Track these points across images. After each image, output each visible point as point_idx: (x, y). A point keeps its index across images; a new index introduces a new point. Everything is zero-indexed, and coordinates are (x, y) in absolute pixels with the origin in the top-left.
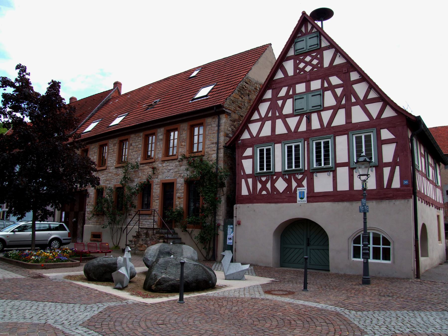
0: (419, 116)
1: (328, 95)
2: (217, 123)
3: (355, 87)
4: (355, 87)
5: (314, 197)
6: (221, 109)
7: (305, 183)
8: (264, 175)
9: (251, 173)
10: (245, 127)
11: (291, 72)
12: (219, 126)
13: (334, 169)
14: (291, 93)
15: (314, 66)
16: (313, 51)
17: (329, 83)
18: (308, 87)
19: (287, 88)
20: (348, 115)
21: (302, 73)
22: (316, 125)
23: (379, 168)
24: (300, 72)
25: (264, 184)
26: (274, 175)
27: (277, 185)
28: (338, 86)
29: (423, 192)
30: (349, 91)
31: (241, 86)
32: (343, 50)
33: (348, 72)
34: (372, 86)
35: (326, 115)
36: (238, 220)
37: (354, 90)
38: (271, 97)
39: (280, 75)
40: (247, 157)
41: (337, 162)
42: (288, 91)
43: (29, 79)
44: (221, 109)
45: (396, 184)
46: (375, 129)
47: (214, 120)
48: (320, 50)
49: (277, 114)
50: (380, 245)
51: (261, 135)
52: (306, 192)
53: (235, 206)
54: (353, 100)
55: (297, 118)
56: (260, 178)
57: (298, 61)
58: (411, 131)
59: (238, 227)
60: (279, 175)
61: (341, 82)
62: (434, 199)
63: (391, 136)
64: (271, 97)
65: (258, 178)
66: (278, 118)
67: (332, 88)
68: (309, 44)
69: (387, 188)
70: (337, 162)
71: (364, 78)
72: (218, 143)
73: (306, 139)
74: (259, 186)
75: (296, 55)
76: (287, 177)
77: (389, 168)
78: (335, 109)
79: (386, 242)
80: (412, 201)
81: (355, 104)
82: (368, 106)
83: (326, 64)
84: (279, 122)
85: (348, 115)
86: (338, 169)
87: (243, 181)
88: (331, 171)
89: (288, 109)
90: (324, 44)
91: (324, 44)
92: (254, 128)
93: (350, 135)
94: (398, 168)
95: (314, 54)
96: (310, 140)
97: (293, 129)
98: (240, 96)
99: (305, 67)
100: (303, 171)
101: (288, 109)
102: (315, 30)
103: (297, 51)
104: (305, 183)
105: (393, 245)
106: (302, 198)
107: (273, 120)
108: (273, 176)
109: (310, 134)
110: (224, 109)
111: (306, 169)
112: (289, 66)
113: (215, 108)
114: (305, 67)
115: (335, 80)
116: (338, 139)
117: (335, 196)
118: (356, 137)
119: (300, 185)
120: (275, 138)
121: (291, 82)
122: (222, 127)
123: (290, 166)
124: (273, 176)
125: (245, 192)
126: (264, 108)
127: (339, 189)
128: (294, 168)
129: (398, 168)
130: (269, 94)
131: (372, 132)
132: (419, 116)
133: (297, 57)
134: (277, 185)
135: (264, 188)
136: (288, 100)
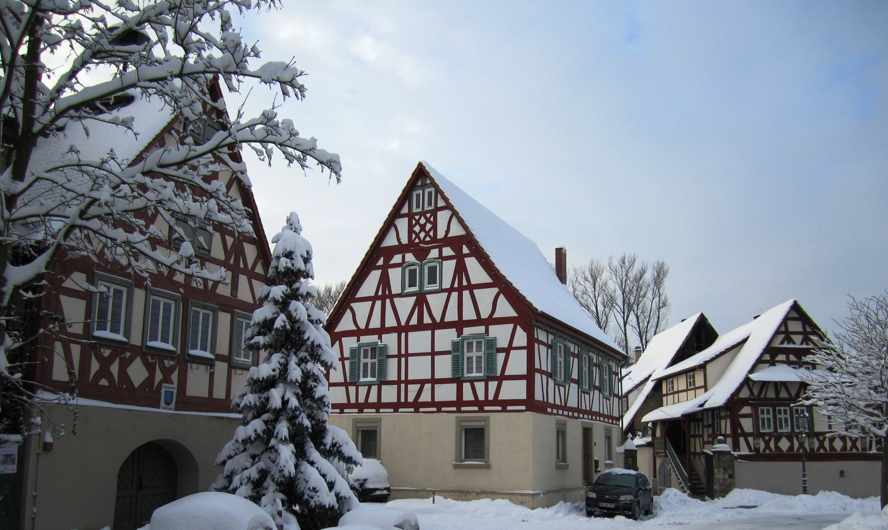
5: (185, 402)
7: (175, 376)
25: (105, 363)
41: (81, 333)
43: (324, 422)
52: (175, 391)
74: (95, 366)
87: (58, 346)
104: (175, 376)
106: (168, 403)
119: (167, 379)
127: (430, 332)
129: (499, 374)
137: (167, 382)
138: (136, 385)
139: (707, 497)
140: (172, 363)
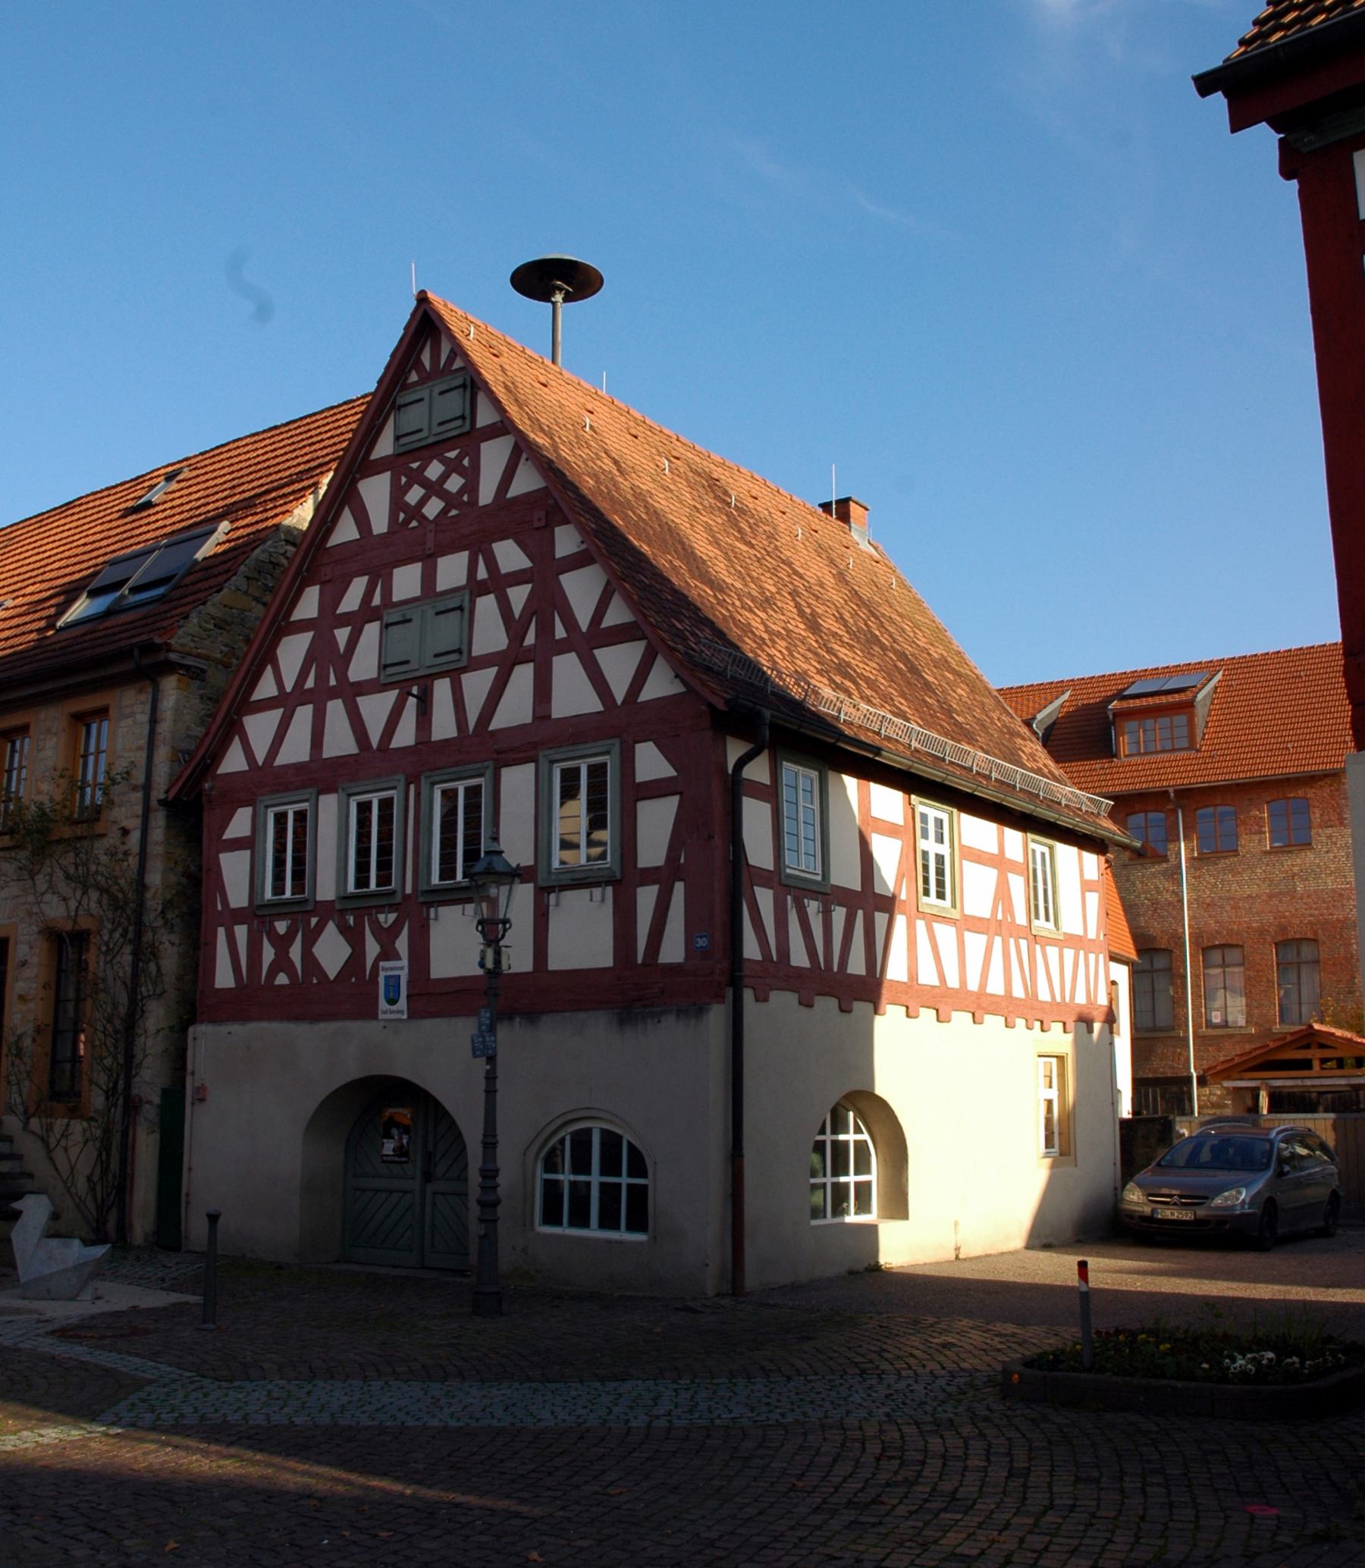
2: (148, 708)
3: (567, 580)
4: (567, 580)
5: (433, 998)
6: (162, 656)
7: (402, 944)
8: (279, 909)
9: (245, 904)
10: (232, 728)
11: (380, 524)
12: (154, 721)
14: (377, 600)
17: (492, 564)
18: (429, 578)
19: (366, 578)
21: (414, 524)
22: (444, 726)
24: (407, 521)
25: (282, 944)
26: (312, 913)
28: (518, 578)
30: (549, 602)
31: (264, 557)
33: (548, 528)
35: (477, 684)
36: (198, 1084)
39: (346, 531)
40: (237, 844)
44: (162, 656)
45: (673, 950)
46: (617, 742)
47: (143, 697)
48: (471, 438)
49: (333, 682)
51: (281, 760)
53: (191, 1029)
54: (560, 632)
55: (392, 695)
56: (271, 923)
57: (404, 480)
60: (326, 911)
67: (498, 584)
68: (438, 417)
69: (644, 964)
72: (147, 787)
74: (268, 954)
75: (399, 455)
78: (504, 664)
81: (563, 647)
82: (605, 656)
83: (486, 494)
87: (221, 932)
89: (364, 666)
92: (260, 728)
94: (679, 888)
95: (452, 454)
96: (423, 779)
98: (256, 599)
99: (423, 502)
100: (398, 899)
101: (364, 666)
103: (403, 441)
104: (402, 944)
108: (307, 914)
109: (427, 759)
111: (409, 890)
112: (375, 492)
113: (136, 653)
115: (510, 556)
118: (563, 771)
119: (388, 953)
120: (322, 775)
121: (376, 558)
122: (165, 727)
123: (362, 881)
124: (307, 914)
125: (224, 978)
126: (293, 651)
128: (373, 886)
129: (679, 888)
135: (282, 962)
139: (16, 1205)
140: (392, 917)
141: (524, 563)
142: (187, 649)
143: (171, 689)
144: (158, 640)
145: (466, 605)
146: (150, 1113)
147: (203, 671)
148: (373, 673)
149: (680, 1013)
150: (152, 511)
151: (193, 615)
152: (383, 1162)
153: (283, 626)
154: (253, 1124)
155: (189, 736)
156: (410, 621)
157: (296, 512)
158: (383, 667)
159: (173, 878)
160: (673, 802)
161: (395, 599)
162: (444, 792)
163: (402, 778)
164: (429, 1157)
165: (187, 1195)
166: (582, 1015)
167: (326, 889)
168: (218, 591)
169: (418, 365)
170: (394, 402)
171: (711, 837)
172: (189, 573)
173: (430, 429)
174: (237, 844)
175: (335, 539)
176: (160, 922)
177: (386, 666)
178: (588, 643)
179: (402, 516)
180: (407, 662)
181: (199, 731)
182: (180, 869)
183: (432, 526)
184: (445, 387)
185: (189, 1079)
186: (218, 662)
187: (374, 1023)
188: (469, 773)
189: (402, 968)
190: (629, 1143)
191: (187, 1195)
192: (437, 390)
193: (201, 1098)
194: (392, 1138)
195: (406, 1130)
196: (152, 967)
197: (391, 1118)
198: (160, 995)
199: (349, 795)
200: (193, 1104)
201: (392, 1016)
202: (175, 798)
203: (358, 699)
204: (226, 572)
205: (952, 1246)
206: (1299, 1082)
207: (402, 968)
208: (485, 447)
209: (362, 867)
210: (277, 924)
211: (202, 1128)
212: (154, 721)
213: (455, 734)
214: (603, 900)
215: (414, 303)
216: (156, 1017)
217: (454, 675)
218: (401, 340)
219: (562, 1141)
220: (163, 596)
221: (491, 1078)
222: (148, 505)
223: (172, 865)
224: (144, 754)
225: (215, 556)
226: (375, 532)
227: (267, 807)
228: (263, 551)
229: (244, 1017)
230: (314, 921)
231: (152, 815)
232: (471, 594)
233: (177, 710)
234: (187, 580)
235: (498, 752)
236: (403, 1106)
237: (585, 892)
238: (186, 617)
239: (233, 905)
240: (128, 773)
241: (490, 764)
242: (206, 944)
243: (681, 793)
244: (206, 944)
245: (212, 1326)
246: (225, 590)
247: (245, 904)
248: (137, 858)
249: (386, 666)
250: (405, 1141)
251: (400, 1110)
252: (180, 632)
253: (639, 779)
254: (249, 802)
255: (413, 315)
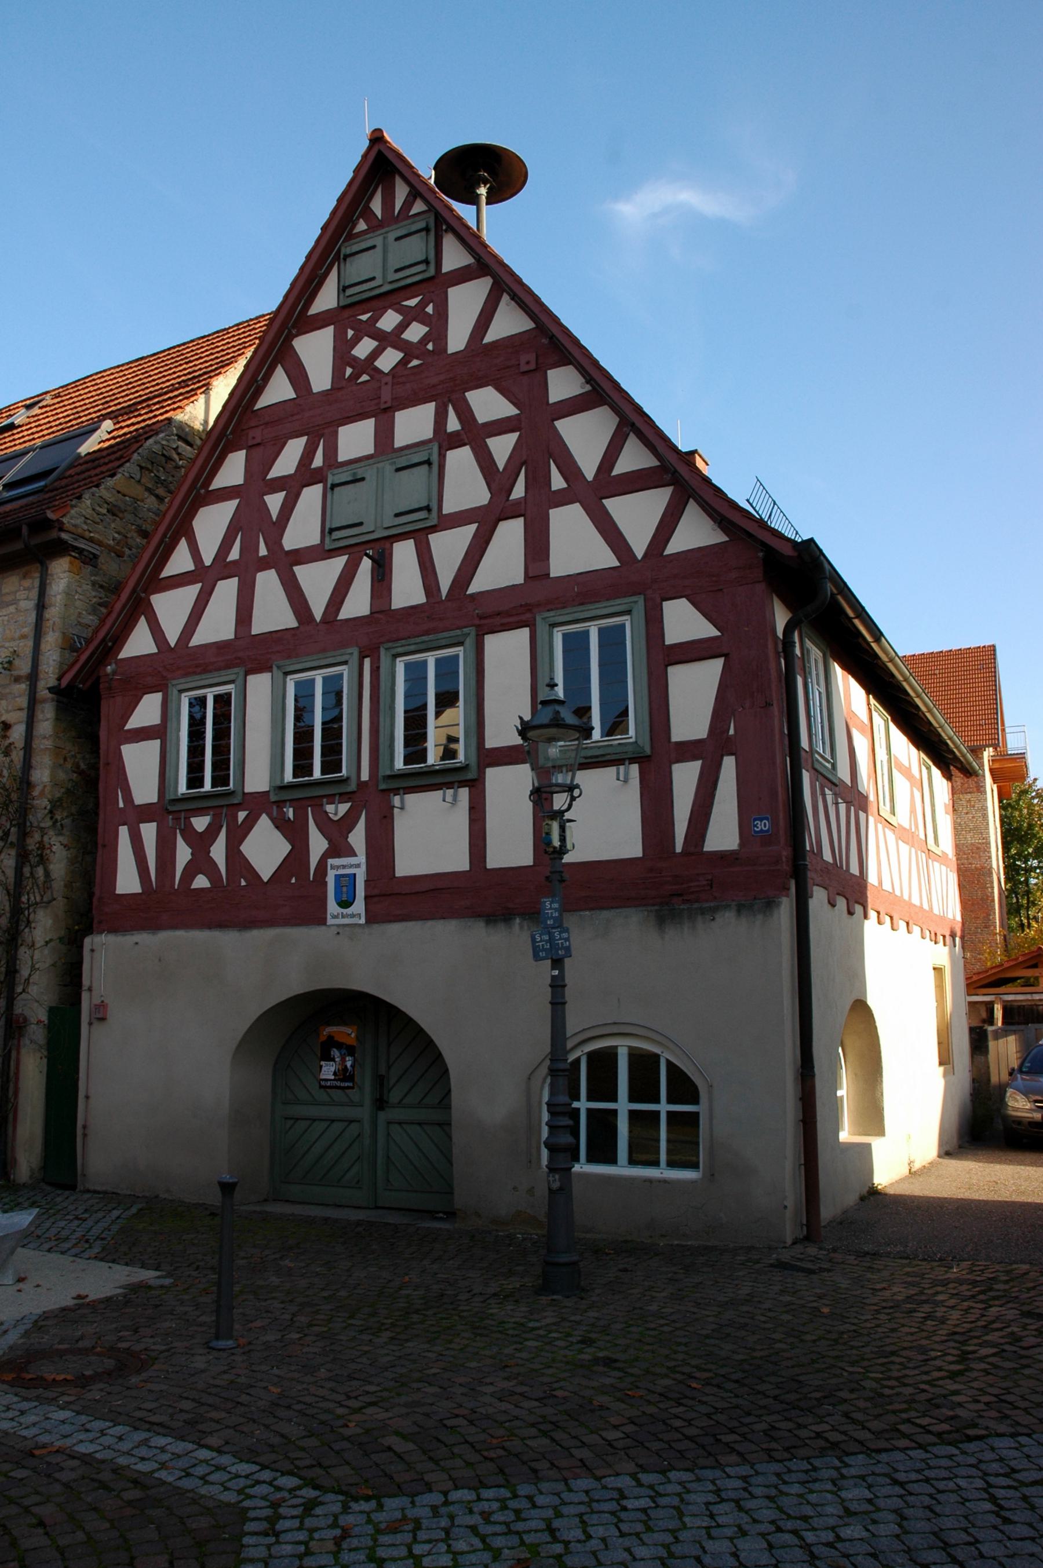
0: (812, 540)
1: (461, 460)
2: (34, 594)
3: (565, 427)
4: (565, 427)
6: (54, 534)
7: (357, 838)
8: (196, 804)
9: (154, 799)
10: (139, 607)
11: (321, 379)
12: (41, 606)
13: (471, 775)
14: (318, 461)
15: (409, 350)
16: (408, 290)
17: (466, 414)
18: (384, 435)
19: (304, 440)
20: (537, 546)
21: (365, 378)
22: (407, 589)
23: (654, 760)
24: (355, 376)
25: (201, 843)
26: (239, 806)
27: (249, 848)
28: (499, 427)
29: (854, 870)
30: (540, 448)
31: (156, 448)
32: (519, 281)
33: (539, 373)
34: (634, 422)
35: (449, 547)
36: (96, 1001)
37: (566, 445)
38: (240, 481)
39: (279, 389)
40: (143, 734)
41: (489, 745)
42: (308, 455)
44: (54, 534)
45: (723, 834)
46: (641, 600)
47: (27, 583)
48: (435, 285)
49: (263, 551)
50: (657, 1101)
51: (198, 639)
53: (87, 941)
54: (558, 482)
55: (339, 563)
56: (187, 819)
57: (350, 333)
58: (788, 605)
59: (98, 1029)
60: (258, 804)
61: (510, 410)
62: (916, 901)
63: (706, 630)
64: (240, 481)
65: (177, 819)
66: (264, 564)
67: (475, 435)
68: (394, 263)
69: (685, 853)
70: (489, 745)
71: (602, 391)
72: (33, 677)
73: (370, 651)
74: (183, 854)
75: (345, 307)
76: (290, 813)
77: (696, 766)
78: (485, 522)
79: (683, 1088)
80: (786, 907)
81: (562, 499)
82: (615, 506)
83: (457, 340)
84: (268, 582)
85: (537, 546)
86: (493, 774)
87: (124, 831)
88: (462, 784)
89: (303, 529)
90: (454, 257)
91: (454, 257)
92: (171, 608)
93: (541, 627)
94: (729, 764)
95: (412, 302)
96: (382, 651)
97: (318, 612)
98: (148, 489)
99: (375, 354)
100: (352, 787)
101: (303, 529)
102: (419, 207)
103: (349, 292)
104: (357, 838)
105: (711, 1100)
106: (345, 904)
107: (245, 573)
108: (234, 810)
109: (386, 631)
110: (64, 536)
111: (365, 776)
112: (316, 350)
113: (25, 530)
114: (375, 354)
115: (488, 404)
116: (493, 643)
117: (476, 895)
118: (566, 637)
119: (339, 848)
120: (250, 652)
121: (316, 418)
122: (54, 613)
123: (302, 766)
124: (234, 810)
125: (127, 881)
126: (211, 524)
128: (317, 773)
129: (729, 764)
130: (233, 471)
131: (628, 612)
132: (812, 540)
133: (347, 313)
134: (249, 848)
135: (201, 862)
136: (305, 490)
137: (338, 855)
138: (266, 876)
140: (344, 808)
141: (509, 410)
142: (80, 531)
143: (62, 574)
144: (50, 515)
145: (435, 458)
146: (36, 1033)
147: (95, 556)
148: (315, 539)
149: (740, 909)
150: (15, 431)
151: (86, 495)
152: (321, 1087)
153: (203, 495)
154: (166, 1045)
155: (79, 623)
156: (363, 479)
157: (188, 409)
158: (327, 531)
159: (62, 776)
160: (716, 666)
161: (340, 459)
162: (408, 666)
163: (355, 651)
164: (380, 1081)
165: (85, 1127)
166: (605, 914)
167: (257, 778)
168: (113, 475)
169: (367, 213)
170: (339, 250)
171: (768, 705)
172: (71, 466)
173: (384, 277)
174: (143, 734)
175: (265, 400)
176: (48, 823)
177: (332, 531)
178: (594, 494)
179: (349, 371)
180: (361, 524)
181: (91, 619)
182: (69, 765)
183: (389, 379)
184: (399, 233)
185: (85, 996)
186: (110, 549)
187: (323, 928)
188: (443, 642)
189: (358, 866)
190: (669, 1063)
191: (85, 1127)
192: (392, 236)
193: (100, 1015)
194: (333, 1060)
195: (351, 1050)
196: (40, 871)
197: (330, 1037)
198: (49, 902)
199: (286, 674)
200: (90, 1024)
201: (346, 921)
202: (68, 685)
203: (297, 569)
204: (118, 459)
205: (906, 1162)
206: (1029, 997)
207: (358, 866)
208: (453, 293)
209: (303, 754)
210: (193, 820)
211: (100, 1051)
212: (41, 606)
213: (424, 600)
214: (626, 781)
215: (367, 143)
216: (44, 927)
217: (420, 536)
218: (350, 184)
219: (578, 1061)
220: (46, 486)
221: (558, 986)
222: (12, 427)
223: (62, 762)
224: (30, 643)
225: (100, 450)
226: (315, 390)
227: (181, 691)
228: (156, 442)
229: (154, 926)
230: (242, 815)
231: (39, 707)
232: (440, 448)
233: (68, 594)
234: (72, 472)
235: (481, 617)
236: (345, 1023)
237: (613, 770)
238: (79, 498)
239: (139, 800)
240: (10, 662)
241: (472, 631)
242: (104, 846)
243: (726, 655)
244: (104, 846)
245: (230, 1343)
246: (119, 476)
247: (154, 799)
248: (22, 753)
249: (332, 531)
250: (349, 1064)
251: (342, 1029)
252: (73, 512)
253: (669, 640)
254: (160, 686)
255: (365, 156)
